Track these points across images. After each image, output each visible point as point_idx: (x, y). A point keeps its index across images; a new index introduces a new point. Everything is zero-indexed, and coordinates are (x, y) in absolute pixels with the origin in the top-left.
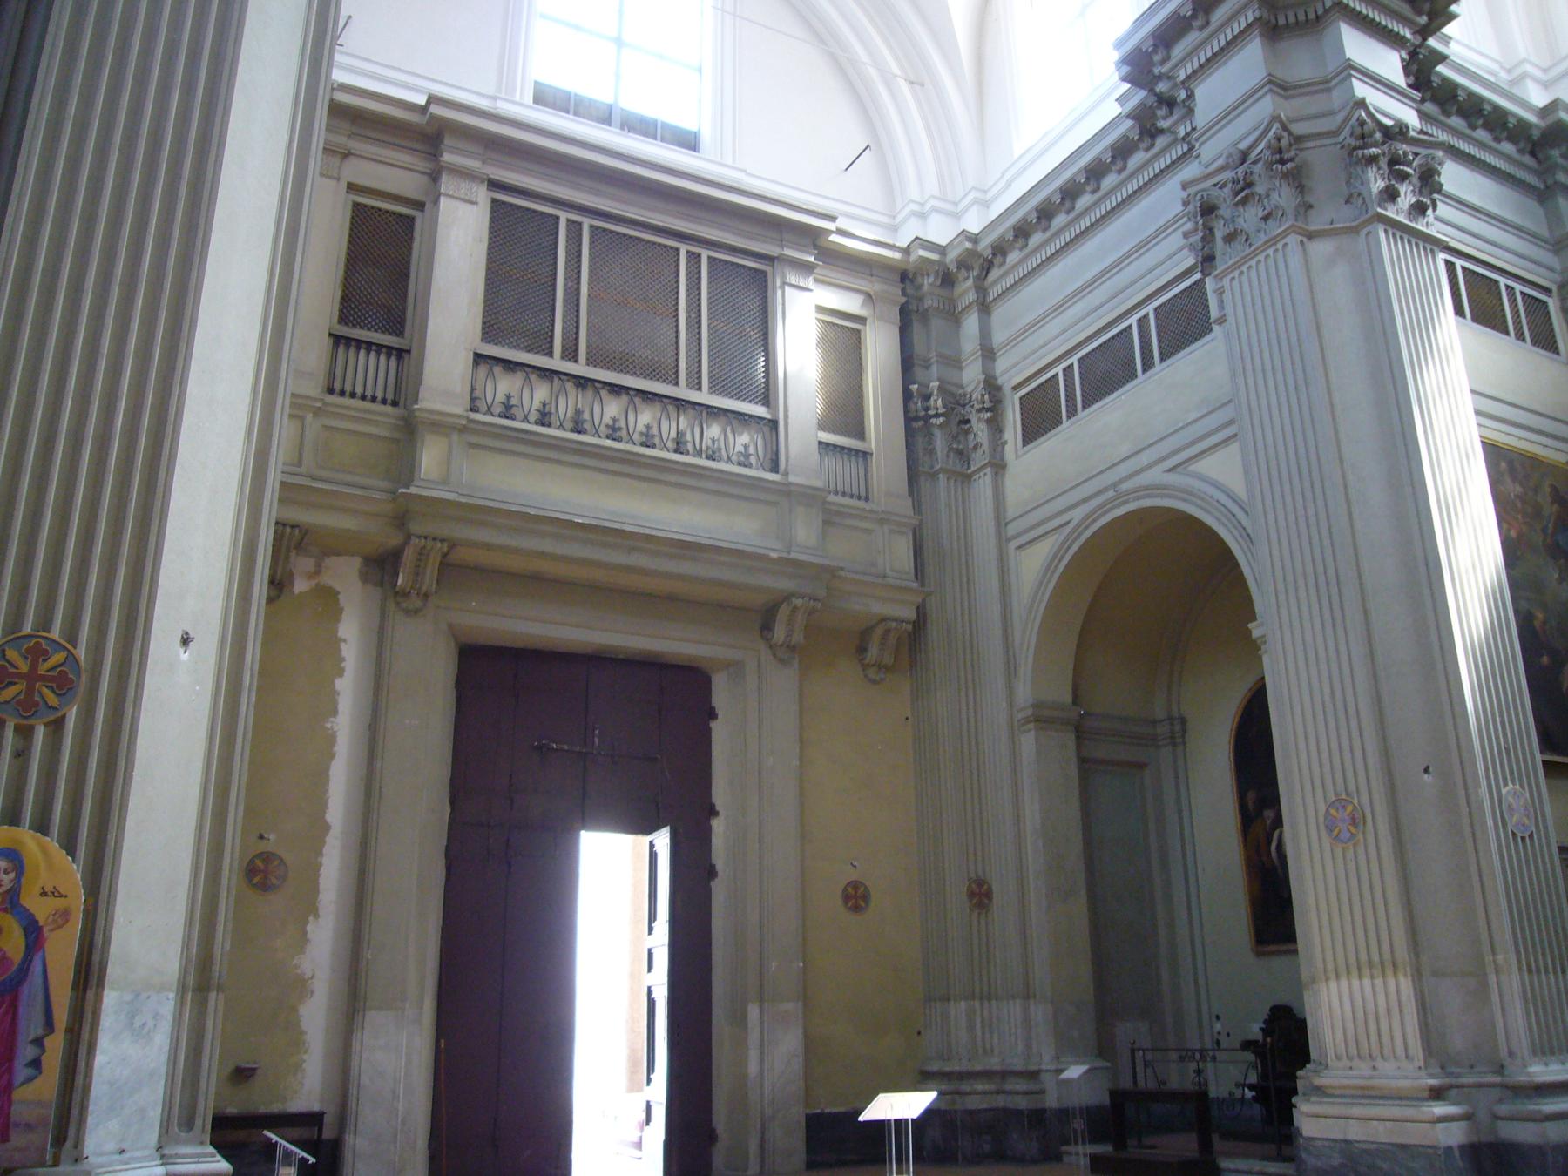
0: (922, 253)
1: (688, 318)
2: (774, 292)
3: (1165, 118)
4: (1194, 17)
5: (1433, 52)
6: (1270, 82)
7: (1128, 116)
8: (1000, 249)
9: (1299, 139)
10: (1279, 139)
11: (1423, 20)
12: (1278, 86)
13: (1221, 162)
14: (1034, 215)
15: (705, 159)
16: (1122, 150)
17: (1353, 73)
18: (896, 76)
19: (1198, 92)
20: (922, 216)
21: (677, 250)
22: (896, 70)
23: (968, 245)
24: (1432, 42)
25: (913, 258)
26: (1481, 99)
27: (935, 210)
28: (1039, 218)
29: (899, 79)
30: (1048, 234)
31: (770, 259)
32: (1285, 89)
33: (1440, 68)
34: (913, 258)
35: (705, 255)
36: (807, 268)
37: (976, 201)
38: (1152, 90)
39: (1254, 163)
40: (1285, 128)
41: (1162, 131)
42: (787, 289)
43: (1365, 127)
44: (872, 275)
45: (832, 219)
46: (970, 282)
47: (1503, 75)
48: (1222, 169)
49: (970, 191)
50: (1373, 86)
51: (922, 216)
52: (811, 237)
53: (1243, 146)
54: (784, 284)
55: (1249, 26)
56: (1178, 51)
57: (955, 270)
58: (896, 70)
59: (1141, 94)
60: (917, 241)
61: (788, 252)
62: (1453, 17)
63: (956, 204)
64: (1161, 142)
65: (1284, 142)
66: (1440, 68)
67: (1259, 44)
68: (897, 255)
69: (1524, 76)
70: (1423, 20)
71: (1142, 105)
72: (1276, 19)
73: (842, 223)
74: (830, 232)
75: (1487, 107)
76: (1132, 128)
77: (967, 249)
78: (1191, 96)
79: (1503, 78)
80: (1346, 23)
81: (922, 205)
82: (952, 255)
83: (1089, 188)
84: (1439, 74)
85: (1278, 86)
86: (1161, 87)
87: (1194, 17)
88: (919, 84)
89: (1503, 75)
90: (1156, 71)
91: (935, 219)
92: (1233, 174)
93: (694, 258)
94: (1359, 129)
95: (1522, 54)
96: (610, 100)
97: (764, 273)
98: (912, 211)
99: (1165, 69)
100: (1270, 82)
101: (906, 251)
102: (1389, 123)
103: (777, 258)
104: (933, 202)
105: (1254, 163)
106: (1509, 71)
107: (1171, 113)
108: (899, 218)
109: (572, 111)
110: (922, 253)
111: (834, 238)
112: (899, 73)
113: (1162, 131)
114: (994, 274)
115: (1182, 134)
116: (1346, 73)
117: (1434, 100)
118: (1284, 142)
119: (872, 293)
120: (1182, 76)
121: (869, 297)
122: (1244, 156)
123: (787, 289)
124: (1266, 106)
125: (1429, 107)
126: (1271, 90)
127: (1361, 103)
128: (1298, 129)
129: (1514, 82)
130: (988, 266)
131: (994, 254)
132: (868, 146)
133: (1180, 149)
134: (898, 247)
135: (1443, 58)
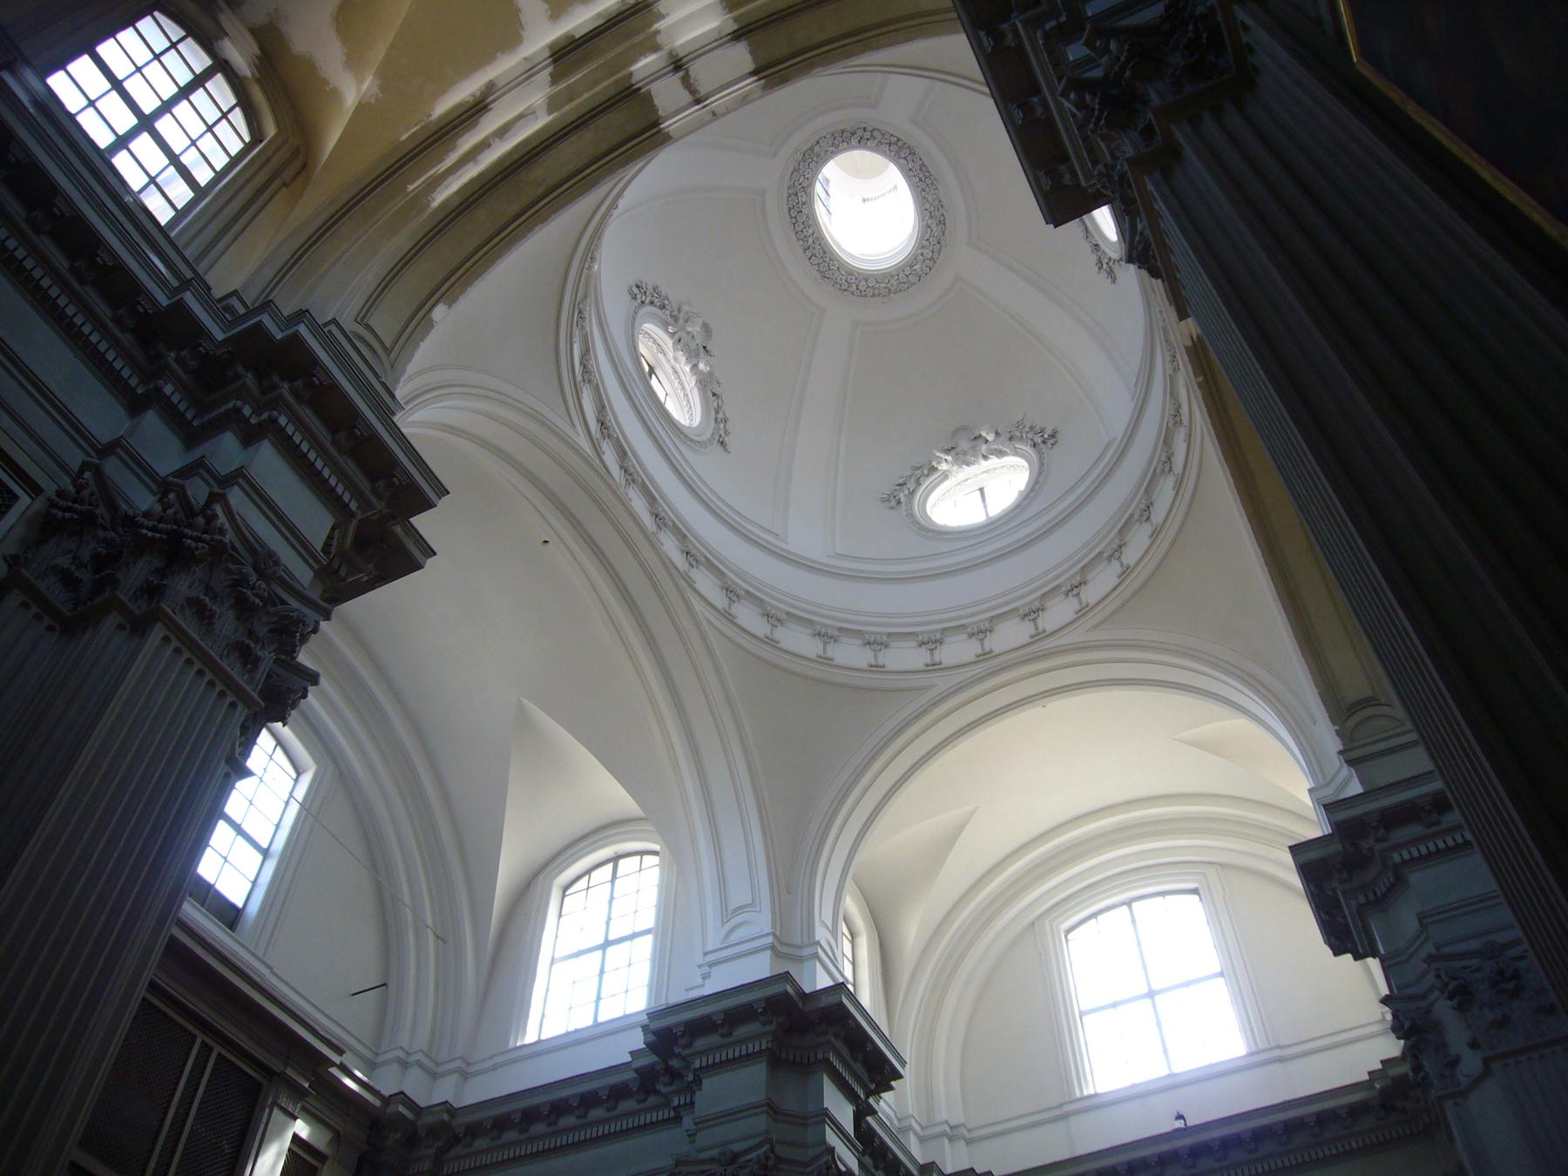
0: (401, 1109)
1: (176, 1113)
2: (263, 1110)
3: (665, 1085)
4: (722, 1025)
5: (870, 1106)
6: (768, 1104)
7: (636, 1071)
8: (474, 1131)
9: (779, 1160)
10: (767, 1158)
11: (873, 1086)
12: (772, 1109)
13: (714, 1153)
14: (520, 1115)
15: (236, 940)
16: (619, 1093)
17: (827, 1119)
18: (428, 927)
19: (706, 1082)
20: (405, 1065)
21: (195, 1037)
22: (430, 922)
23: (446, 1117)
24: (871, 1100)
25: (391, 1109)
26: (888, 1149)
27: (419, 1064)
28: (522, 1119)
29: (429, 931)
30: (523, 1137)
31: (270, 1073)
32: (776, 1113)
33: (869, 1119)
34: (391, 1109)
35: (217, 1049)
36: (298, 1093)
37: (458, 1071)
38: (665, 1061)
39: (741, 1167)
40: (772, 1150)
41: (657, 1092)
42: (276, 1111)
43: (830, 1171)
44: (348, 1115)
45: (340, 1052)
46: (431, 1151)
47: (896, 1122)
48: (712, 1160)
49: (454, 1059)
50: (836, 1134)
51: (405, 1065)
52: (315, 1063)
53: (737, 1147)
54: (275, 1104)
55: (761, 1051)
56: (701, 1043)
57: (423, 1135)
58: (430, 922)
59: (652, 1059)
60: (402, 1096)
61: (289, 1071)
62: (891, 1088)
63: (438, 1064)
64: (652, 1100)
65: (770, 1163)
66: (869, 1119)
67: (765, 1070)
68: (377, 1103)
69: (910, 1128)
70: (873, 1086)
71: (651, 1068)
72: (339, 567)
73: (347, 1059)
74: (333, 1064)
75: (890, 1156)
76: (634, 1079)
77: (444, 1120)
78: (698, 1081)
79: (894, 1124)
80: (272, 443)
81: (408, 1054)
82: (429, 1119)
83: (577, 1113)
84: (867, 1122)
85: (772, 1109)
86: (674, 1063)
87: (722, 1025)
88: (442, 940)
89: (896, 1122)
90: (677, 1050)
91: (415, 1074)
92: (722, 1169)
93: (206, 1050)
94: (826, 1171)
95: (911, 1112)
96: (212, 882)
97: (260, 1085)
98: (398, 1057)
99: (685, 1052)
100: (768, 1104)
101: (387, 1100)
102: (843, 1169)
103: (279, 1075)
104: (419, 1056)
105: (741, 1167)
106: (899, 1120)
107: (672, 1083)
108: (381, 1058)
109: (206, 906)
110: (401, 1109)
111: (334, 1070)
112: (431, 926)
113: (657, 1092)
114: (459, 1150)
115: (675, 1103)
116: (820, 1118)
117: (872, 1156)
118: (770, 1163)
119: (342, 1133)
120: (697, 1065)
121: (337, 1138)
122: (735, 1157)
123: (276, 1111)
124: (760, 1122)
125: (867, 1160)
126: (767, 1112)
127: (831, 1150)
128: (782, 1151)
129: (900, 1129)
130: (454, 1140)
131: (465, 1135)
132: (385, 985)
133: (667, 1114)
134: (381, 1095)
135: (873, 1112)
